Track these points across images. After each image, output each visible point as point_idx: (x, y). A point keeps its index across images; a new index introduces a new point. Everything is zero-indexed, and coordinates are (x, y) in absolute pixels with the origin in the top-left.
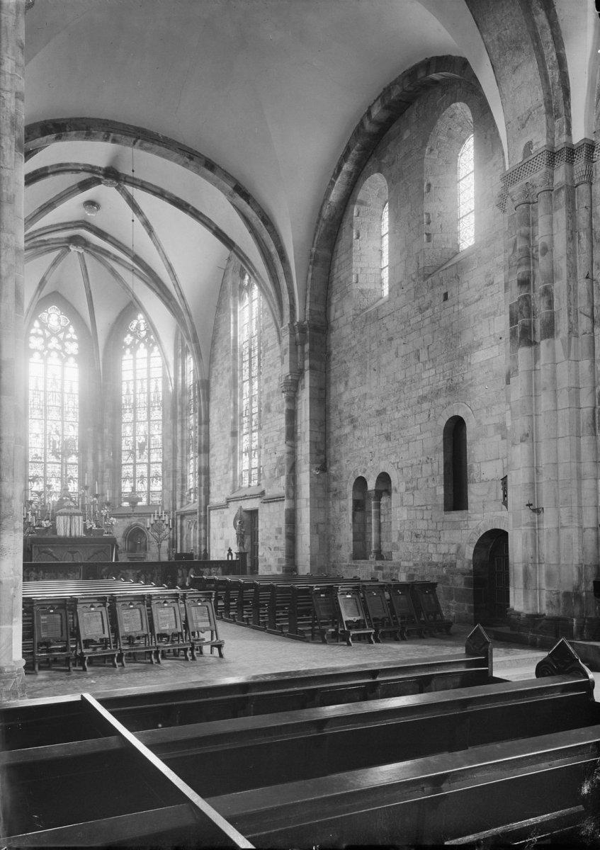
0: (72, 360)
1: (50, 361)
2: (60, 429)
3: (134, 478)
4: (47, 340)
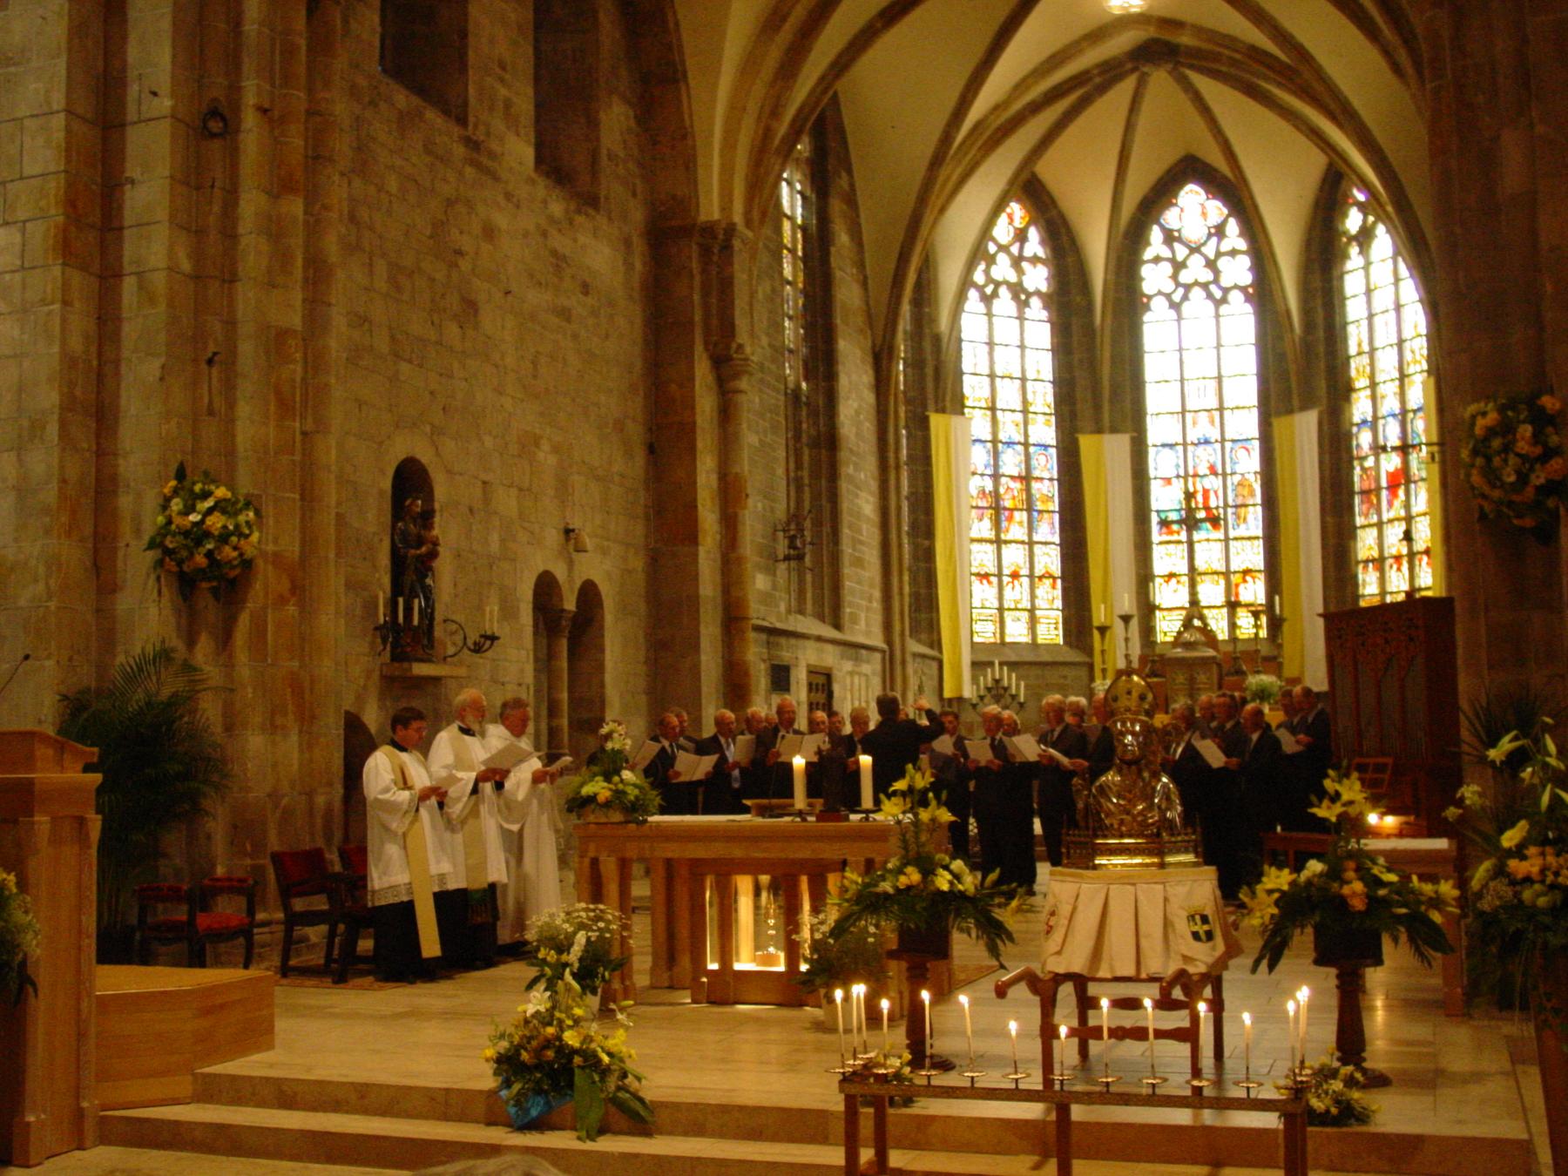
1: (997, 305)
4: (1178, 266)
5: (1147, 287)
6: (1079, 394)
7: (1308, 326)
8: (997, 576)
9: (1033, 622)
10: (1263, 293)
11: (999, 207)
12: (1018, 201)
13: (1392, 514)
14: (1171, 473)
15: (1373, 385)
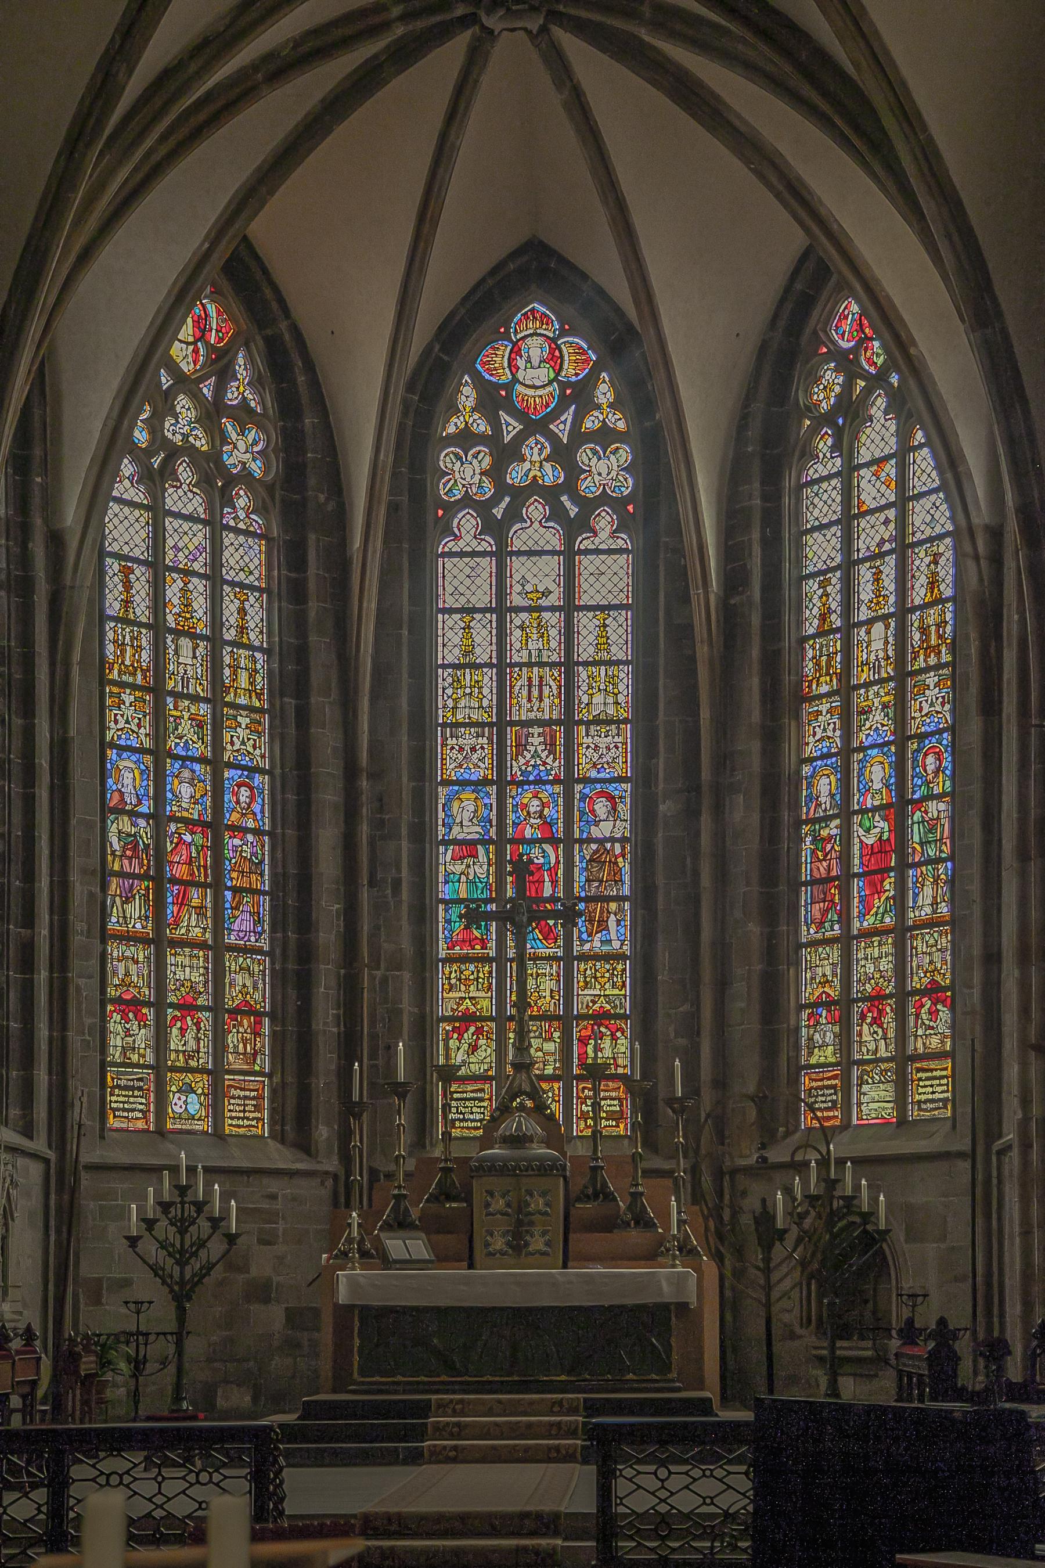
0: (604, 521)
1: (520, 538)
2: (555, 813)
3: (159, 1004)
4: (506, 454)
5: (449, 490)
6: (316, 677)
7: (734, 580)
8: (158, 1007)
9: (216, 1097)
10: (653, 510)
11: (182, 298)
12: (217, 294)
13: (869, 921)
14: (473, 832)
15: (846, 690)
